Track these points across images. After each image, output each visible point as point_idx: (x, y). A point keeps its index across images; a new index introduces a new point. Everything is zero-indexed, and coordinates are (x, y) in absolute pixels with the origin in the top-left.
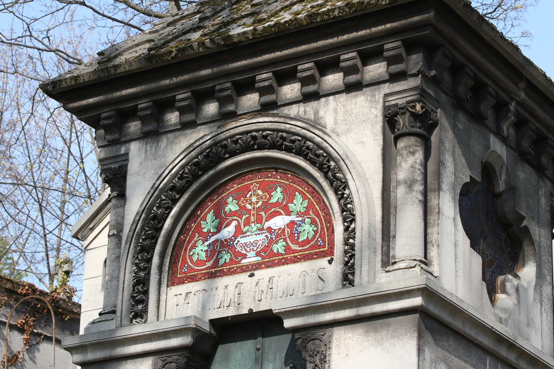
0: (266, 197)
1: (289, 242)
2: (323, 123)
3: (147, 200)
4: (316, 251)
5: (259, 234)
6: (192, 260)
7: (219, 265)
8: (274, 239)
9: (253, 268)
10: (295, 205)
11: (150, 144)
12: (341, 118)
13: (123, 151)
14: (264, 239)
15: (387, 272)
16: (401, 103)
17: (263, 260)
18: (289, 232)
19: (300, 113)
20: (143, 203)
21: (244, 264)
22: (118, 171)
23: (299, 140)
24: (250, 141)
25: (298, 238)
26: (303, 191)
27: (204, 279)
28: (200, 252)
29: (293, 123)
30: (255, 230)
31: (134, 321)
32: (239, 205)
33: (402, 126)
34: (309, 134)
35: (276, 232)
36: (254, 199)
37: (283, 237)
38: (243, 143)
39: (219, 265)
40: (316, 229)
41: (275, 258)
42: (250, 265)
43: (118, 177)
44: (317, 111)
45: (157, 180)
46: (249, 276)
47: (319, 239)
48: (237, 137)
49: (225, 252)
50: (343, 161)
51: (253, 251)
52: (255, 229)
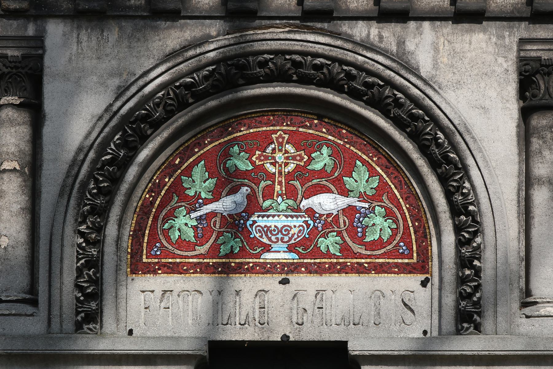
0: (302, 159)
1: (347, 239)
2: (413, 61)
3: (97, 130)
4: (396, 261)
5: (292, 217)
6: (168, 239)
7: (220, 255)
8: (320, 229)
9: (283, 269)
10: (356, 181)
11: (87, 30)
12: (445, 60)
13: (31, 31)
14: (302, 226)
15: (527, 317)
16: (546, 58)
17: (302, 261)
18: (347, 223)
19: (372, 37)
20: (89, 133)
21: (268, 261)
22: (20, 62)
23: (379, 85)
24: (289, 69)
25: (364, 236)
26: (370, 161)
27: (193, 273)
28: (184, 227)
29: (369, 55)
30: (285, 208)
31: (85, 327)
32: (253, 163)
33: (542, 91)
34: (399, 80)
35: (323, 218)
36: (279, 157)
37: (336, 229)
38: (276, 69)
39: (220, 255)
40: (394, 226)
41: (324, 260)
42: (279, 263)
43: (21, 73)
44: (402, 40)
45: (117, 99)
46: (280, 282)
47: (402, 244)
48: (265, 56)
49: (230, 235)
50: (461, 135)
51: (282, 242)
52: (283, 206)
